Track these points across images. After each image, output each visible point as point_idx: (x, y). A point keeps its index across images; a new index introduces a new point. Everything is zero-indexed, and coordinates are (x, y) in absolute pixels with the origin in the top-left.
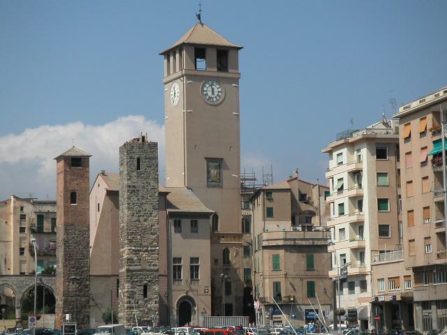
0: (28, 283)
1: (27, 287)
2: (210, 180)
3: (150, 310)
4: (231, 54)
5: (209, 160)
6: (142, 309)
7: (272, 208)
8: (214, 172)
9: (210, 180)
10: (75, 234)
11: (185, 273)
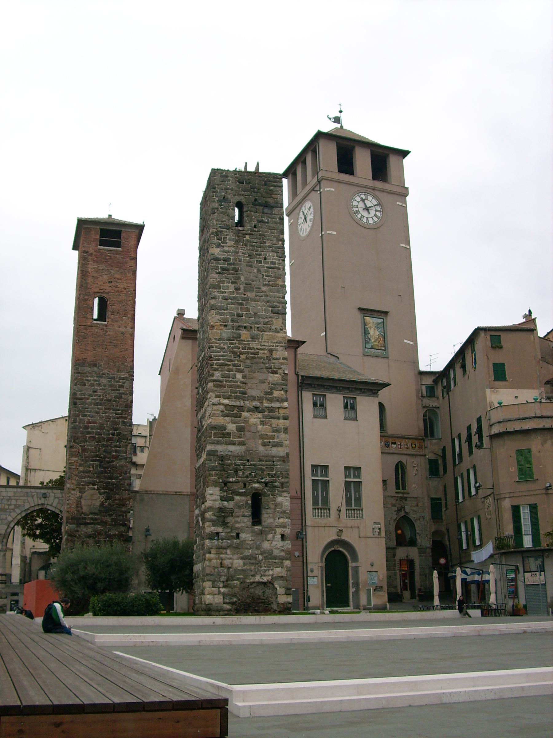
0: (20, 503)
1: (18, 511)
2: (369, 346)
3: (269, 555)
4: (392, 160)
5: (364, 311)
6: (248, 552)
7: (503, 365)
8: (374, 333)
9: (369, 346)
10: (99, 385)
11: (337, 494)
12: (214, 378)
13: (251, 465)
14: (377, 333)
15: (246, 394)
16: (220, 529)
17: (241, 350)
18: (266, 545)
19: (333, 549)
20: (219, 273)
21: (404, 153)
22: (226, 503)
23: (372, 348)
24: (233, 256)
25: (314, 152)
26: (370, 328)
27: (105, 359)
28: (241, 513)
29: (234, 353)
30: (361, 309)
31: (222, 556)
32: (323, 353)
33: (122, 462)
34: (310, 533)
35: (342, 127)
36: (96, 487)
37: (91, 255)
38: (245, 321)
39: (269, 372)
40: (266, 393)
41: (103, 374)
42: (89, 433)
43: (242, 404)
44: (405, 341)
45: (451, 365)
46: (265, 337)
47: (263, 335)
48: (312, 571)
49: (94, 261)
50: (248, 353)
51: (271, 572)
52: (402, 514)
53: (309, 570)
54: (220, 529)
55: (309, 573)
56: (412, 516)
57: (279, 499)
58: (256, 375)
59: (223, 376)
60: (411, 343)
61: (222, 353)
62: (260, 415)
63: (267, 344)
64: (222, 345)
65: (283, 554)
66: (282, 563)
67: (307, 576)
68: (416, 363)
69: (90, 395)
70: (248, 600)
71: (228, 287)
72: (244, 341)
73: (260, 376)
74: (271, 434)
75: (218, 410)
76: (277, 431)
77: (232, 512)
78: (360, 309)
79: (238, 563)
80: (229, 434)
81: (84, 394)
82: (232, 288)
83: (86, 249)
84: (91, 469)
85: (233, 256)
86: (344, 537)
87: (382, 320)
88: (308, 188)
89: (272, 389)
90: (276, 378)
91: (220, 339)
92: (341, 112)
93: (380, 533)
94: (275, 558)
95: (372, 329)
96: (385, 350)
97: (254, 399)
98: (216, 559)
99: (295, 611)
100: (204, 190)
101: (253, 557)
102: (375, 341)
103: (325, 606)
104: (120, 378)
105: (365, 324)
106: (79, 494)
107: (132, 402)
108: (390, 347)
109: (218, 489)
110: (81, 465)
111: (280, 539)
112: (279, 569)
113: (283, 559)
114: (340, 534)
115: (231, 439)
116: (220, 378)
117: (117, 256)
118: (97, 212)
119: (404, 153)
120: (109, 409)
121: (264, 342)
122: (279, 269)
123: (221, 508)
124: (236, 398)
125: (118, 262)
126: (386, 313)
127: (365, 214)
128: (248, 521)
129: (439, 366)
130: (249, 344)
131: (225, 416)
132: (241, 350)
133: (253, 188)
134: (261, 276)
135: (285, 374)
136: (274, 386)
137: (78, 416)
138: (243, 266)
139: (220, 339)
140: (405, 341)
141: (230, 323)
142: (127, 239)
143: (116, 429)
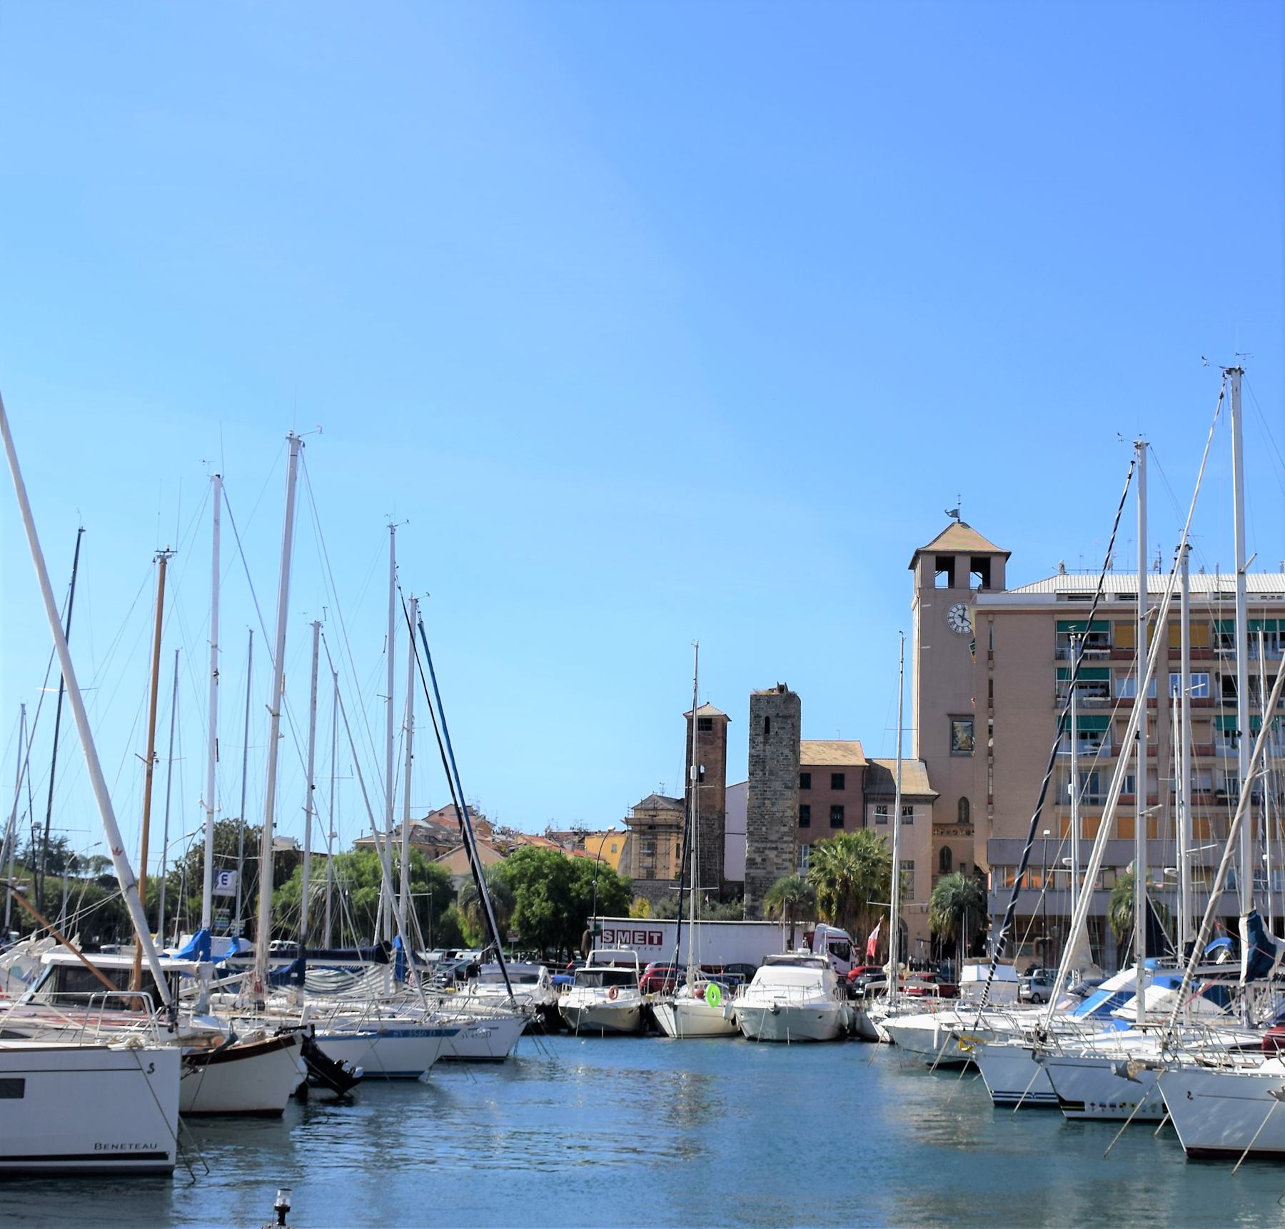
7: (20, 1094)
8: (962, 736)
30: (950, 715)
38: (769, 794)
73: (776, 828)
105: (953, 728)
119: (1008, 555)
127: (958, 621)
136: (785, 834)
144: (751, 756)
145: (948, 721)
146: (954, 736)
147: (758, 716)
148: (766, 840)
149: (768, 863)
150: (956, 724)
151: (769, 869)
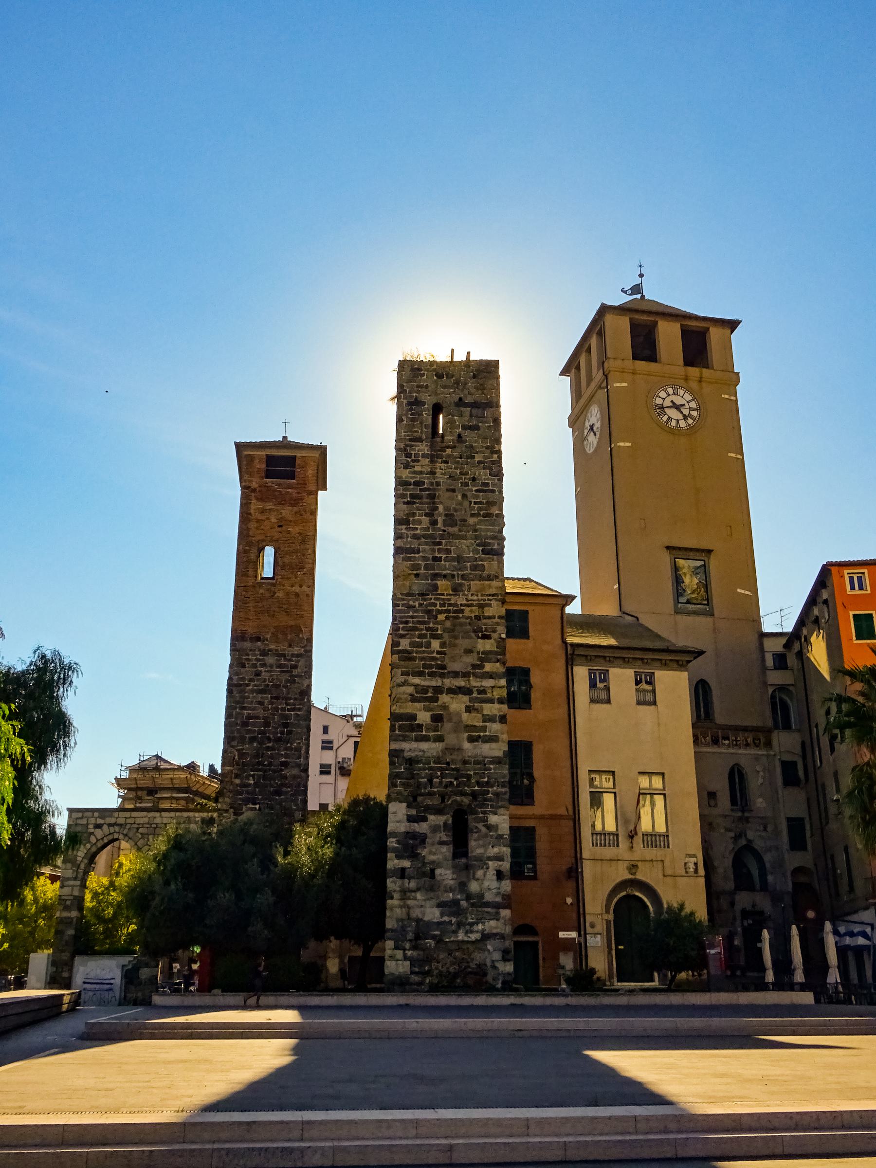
3: (478, 902)
8: (690, 582)
10: (264, 665)
12: (400, 648)
13: (453, 769)
14: (696, 581)
15: (445, 669)
16: (407, 864)
17: (438, 607)
18: (474, 887)
19: (624, 893)
20: (408, 503)
21: (732, 325)
22: (416, 824)
23: (688, 602)
24: (428, 478)
25: (601, 334)
26: (685, 574)
27: (272, 630)
28: (438, 839)
29: (429, 612)
31: (410, 902)
32: (620, 614)
33: (295, 771)
34: (588, 870)
35: (643, 297)
36: (257, 807)
37: (254, 490)
38: (446, 567)
39: (479, 638)
40: (474, 666)
41: (270, 650)
42: (249, 731)
43: (439, 684)
44: (739, 590)
45: (801, 622)
46: (473, 589)
47: (469, 586)
48: (592, 926)
49: (257, 499)
50: (448, 611)
51: (480, 927)
52: (743, 842)
53: (588, 925)
54: (407, 864)
55: (589, 930)
56: (758, 844)
57: (493, 819)
58: (459, 641)
59: (412, 644)
60: (748, 593)
61: (411, 614)
62: (466, 698)
63: (476, 598)
64: (411, 603)
65: (498, 899)
66: (498, 913)
67: (585, 934)
68: (756, 620)
69: (251, 680)
70: (452, 969)
71: (420, 522)
72: (443, 595)
74: (481, 724)
75: (404, 693)
76: (490, 719)
77: (422, 839)
78: (668, 548)
79: (432, 914)
80: (420, 726)
81: (243, 679)
82: (426, 520)
83: (247, 484)
84: (252, 782)
85: (428, 478)
86: (640, 876)
87: (702, 563)
88: (593, 385)
89: (482, 660)
90: (488, 645)
91: (408, 594)
92: (641, 276)
93: (696, 871)
94: (487, 904)
95: (688, 576)
96: (708, 604)
97: (456, 674)
98: (401, 907)
99: (374, 985)
100: (394, 390)
101: (456, 903)
102: (693, 593)
103: (615, 979)
104: (293, 655)
105: (676, 569)
106: (232, 817)
107: (309, 686)
108: (716, 601)
109: (404, 805)
110: (237, 776)
111: (495, 877)
112: (493, 923)
113: (497, 906)
114: (634, 871)
115: (424, 733)
116: (408, 648)
117: (289, 490)
118: (269, 432)
119: (732, 325)
120: (277, 698)
121: (472, 595)
122: (493, 491)
123: (408, 833)
124: (432, 675)
125: (291, 499)
126: (709, 552)
127: (678, 401)
128: (446, 851)
129: (789, 627)
130: (449, 600)
131: (414, 700)
132: (438, 607)
133: (457, 382)
134: (466, 503)
135: (501, 638)
136: (486, 657)
137: (236, 708)
138: (442, 494)
139: (408, 594)
140: (739, 590)
141: (422, 571)
142: (303, 467)
143: (286, 725)
144: (400, 483)
145: (666, 558)
146: (678, 580)
147: (417, 402)
148: (441, 671)
149: (448, 726)
150: (681, 562)
151: (451, 739)
